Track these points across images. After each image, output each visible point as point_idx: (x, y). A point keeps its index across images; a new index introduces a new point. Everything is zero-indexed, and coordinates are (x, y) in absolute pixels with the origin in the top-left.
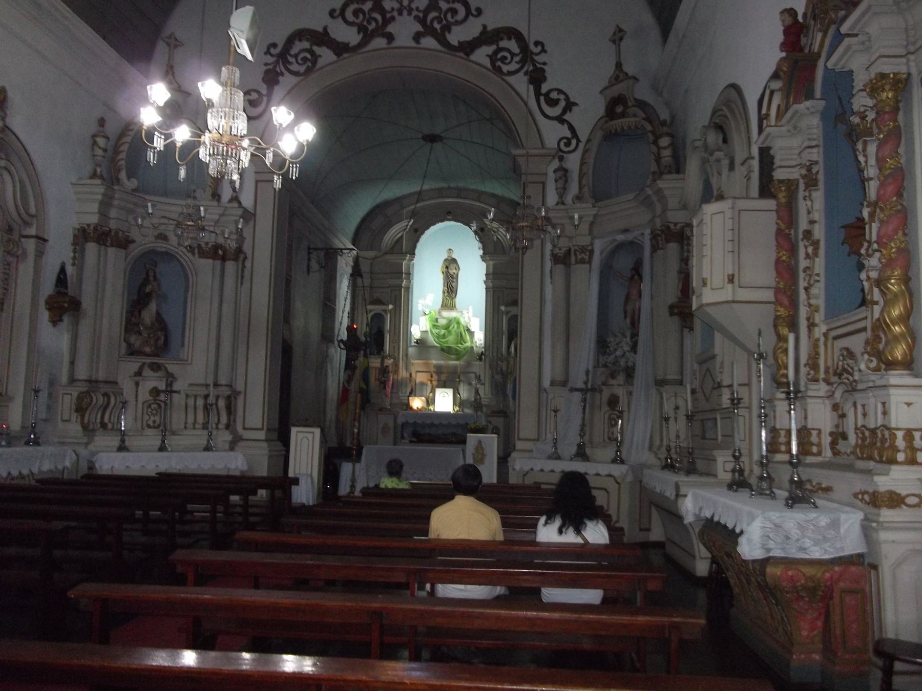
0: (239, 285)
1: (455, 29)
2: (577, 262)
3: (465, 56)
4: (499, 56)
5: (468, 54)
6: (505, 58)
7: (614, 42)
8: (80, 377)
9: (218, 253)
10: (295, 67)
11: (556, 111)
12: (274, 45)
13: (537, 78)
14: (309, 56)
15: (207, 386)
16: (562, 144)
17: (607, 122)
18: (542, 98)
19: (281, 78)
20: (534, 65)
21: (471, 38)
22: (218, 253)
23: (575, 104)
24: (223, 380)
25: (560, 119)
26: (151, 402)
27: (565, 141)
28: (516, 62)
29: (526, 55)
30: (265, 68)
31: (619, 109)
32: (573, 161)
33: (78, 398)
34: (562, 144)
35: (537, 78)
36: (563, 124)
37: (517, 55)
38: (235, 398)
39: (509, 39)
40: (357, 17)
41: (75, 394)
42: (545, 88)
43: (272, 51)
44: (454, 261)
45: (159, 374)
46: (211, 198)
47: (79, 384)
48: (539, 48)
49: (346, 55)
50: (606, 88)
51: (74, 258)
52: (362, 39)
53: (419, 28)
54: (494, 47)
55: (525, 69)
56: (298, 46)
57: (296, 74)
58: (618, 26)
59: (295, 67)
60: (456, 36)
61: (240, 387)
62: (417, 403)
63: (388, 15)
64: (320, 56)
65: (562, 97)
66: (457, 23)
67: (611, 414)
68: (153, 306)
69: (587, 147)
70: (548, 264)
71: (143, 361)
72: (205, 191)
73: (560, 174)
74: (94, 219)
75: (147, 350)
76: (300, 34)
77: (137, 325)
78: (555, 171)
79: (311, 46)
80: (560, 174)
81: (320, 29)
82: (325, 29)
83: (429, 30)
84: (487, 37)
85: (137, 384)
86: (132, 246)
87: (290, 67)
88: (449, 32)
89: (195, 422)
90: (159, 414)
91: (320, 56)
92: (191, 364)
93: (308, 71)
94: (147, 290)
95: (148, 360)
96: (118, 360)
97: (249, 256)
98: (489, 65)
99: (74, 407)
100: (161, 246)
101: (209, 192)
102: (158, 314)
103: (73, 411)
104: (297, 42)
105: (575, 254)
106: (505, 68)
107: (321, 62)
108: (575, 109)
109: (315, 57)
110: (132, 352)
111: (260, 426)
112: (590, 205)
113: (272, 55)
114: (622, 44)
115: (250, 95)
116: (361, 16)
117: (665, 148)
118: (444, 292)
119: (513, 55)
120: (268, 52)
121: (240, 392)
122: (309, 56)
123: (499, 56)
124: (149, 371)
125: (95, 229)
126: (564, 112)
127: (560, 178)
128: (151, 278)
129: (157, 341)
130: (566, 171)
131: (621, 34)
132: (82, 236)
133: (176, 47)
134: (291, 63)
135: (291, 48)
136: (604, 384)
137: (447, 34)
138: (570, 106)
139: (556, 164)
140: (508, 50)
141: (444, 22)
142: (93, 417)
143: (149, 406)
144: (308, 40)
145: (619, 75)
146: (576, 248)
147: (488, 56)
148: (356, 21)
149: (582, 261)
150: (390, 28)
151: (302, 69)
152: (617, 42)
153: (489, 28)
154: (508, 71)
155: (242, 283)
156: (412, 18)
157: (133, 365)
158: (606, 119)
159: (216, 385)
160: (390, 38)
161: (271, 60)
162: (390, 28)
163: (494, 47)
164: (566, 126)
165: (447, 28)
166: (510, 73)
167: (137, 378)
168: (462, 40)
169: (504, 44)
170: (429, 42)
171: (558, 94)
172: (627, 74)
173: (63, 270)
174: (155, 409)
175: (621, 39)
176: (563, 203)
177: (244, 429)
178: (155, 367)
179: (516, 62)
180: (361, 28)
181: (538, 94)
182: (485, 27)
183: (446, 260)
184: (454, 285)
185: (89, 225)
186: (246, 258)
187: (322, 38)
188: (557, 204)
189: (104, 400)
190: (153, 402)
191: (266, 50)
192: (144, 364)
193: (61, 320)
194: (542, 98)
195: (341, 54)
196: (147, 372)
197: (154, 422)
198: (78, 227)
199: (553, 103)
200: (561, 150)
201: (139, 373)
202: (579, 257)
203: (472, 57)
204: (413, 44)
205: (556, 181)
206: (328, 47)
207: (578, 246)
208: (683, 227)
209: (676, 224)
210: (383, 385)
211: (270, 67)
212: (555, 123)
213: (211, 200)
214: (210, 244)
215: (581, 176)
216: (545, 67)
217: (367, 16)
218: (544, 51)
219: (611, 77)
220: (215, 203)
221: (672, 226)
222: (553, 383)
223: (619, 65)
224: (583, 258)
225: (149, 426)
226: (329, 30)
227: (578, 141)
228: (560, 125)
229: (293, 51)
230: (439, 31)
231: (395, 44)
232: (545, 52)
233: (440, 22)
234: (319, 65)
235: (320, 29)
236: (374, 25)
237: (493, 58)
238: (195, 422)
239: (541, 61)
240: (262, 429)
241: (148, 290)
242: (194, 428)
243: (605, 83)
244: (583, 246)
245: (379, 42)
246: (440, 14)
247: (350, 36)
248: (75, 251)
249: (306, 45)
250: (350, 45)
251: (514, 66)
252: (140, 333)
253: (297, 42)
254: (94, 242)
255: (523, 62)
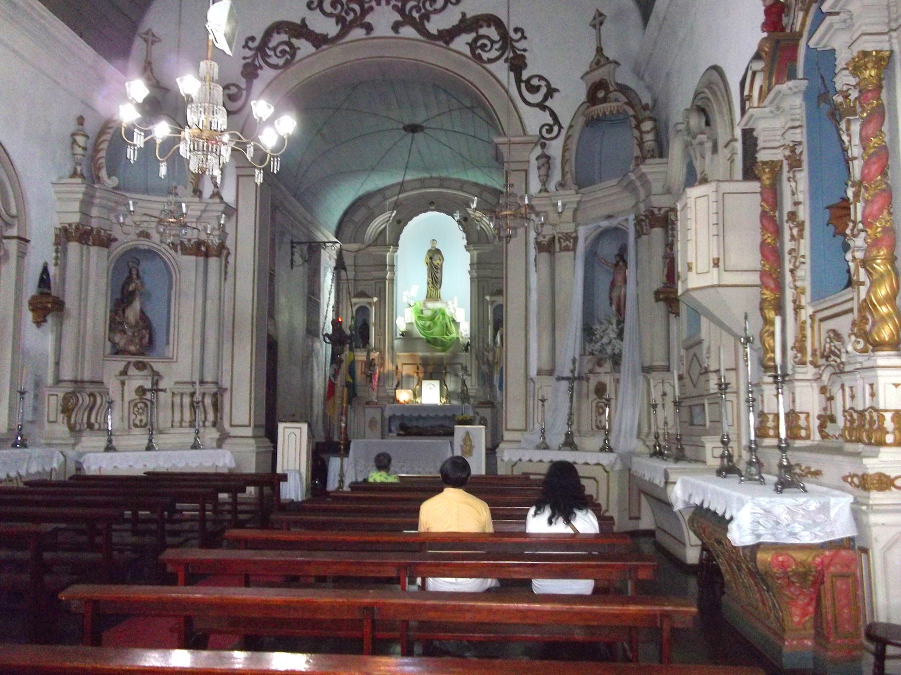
0: (223, 281)
1: (434, 17)
2: (561, 250)
3: (444, 45)
4: (479, 44)
5: (447, 43)
6: (484, 45)
7: (594, 26)
8: (66, 378)
9: (200, 249)
10: (274, 60)
11: (537, 98)
12: (252, 39)
13: (517, 65)
14: (287, 49)
15: (193, 383)
16: (544, 131)
17: (588, 107)
18: (523, 85)
19: (259, 72)
20: (514, 52)
21: (450, 27)
22: (200, 249)
23: (557, 90)
24: (209, 378)
25: (542, 106)
26: (137, 401)
27: (547, 127)
28: (496, 49)
29: (506, 42)
30: (244, 62)
31: (601, 94)
32: (555, 148)
33: (64, 398)
34: (544, 131)
35: (517, 65)
36: (544, 111)
37: (497, 42)
38: (222, 395)
39: (489, 26)
40: (335, 9)
41: (61, 395)
42: (525, 75)
43: (251, 44)
44: (438, 251)
45: (145, 372)
46: (192, 194)
47: (64, 384)
48: (519, 35)
49: (324, 47)
50: (587, 73)
51: (57, 258)
52: (341, 30)
53: (398, 17)
54: (473, 35)
55: (505, 56)
56: (278, 38)
57: (275, 67)
58: (598, 10)
59: (274, 60)
60: (435, 25)
61: (226, 384)
62: (404, 396)
63: (366, 6)
64: (299, 48)
65: (543, 83)
66: (436, 11)
67: (599, 402)
68: (137, 305)
69: (569, 134)
70: (533, 252)
71: (129, 360)
72: (186, 188)
73: (542, 161)
74: (75, 218)
75: (132, 348)
76: (278, 27)
77: (121, 323)
78: (537, 159)
79: (289, 39)
80: (542, 161)
81: (298, 21)
82: (303, 20)
83: (407, 20)
84: (467, 25)
85: (123, 383)
86: (114, 245)
87: (271, 61)
88: (428, 21)
89: (182, 420)
90: (145, 413)
91: (299, 48)
92: (176, 361)
93: (288, 64)
94: (131, 288)
95: (133, 359)
96: (103, 360)
97: (232, 251)
98: (468, 53)
99: (60, 408)
100: (144, 244)
101: (190, 188)
102: (142, 312)
103: (59, 412)
104: (275, 35)
105: (560, 242)
106: (485, 56)
107: (299, 55)
108: (556, 95)
109: (294, 50)
110: (117, 351)
111: (247, 423)
112: (573, 192)
113: (250, 49)
114: (602, 28)
115: (229, 89)
116: (339, 7)
117: (648, 132)
118: (428, 284)
119: (493, 42)
120: (246, 46)
121: (226, 389)
122: (287, 49)
123: (479, 44)
124: (135, 370)
125: (77, 228)
126: (546, 98)
127: (543, 165)
128: (135, 276)
129: (141, 339)
130: (548, 158)
131: (601, 18)
132: (64, 236)
133: (153, 43)
134: (269, 56)
135: (269, 41)
136: (591, 372)
137: (426, 23)
138: (551, 92)
139: (538, 151)
140: (488, 38)
141: (423, 11)
142: (78, 417)
143: (136, 405)
144: (286, 33)
145: (600, 59)
146: (560, 235)
147: (467, 43)
148: (334, 12)
149: (567, 249)
150: (368, 19)
151: (281, 62)
152: (598, 27)
153: (468, 16)
154: (488, 59)
155: (225, 279)
156: (390, 7)
157: (119, 364)
158: (588, 104)
159: (202, 382)
160: (369, 28)
161: (249, 53)
162: (368, 19)
163: (473, 35)
164: (547, 113)
165: (426, 17)
166: (490, 61)
167: (122, 378)
168: (441, 28)
169: (483, 31)
170: (408, 31)
171: (539, 80)
172: (608, 58)
173: (45, 270)
174: (141, 408)
175: (601, 23)
176: (546, 191)
177: (232, 426)
178: (141, 366)
179: (496, 49)
180: (340, 20)
181: (519, 81)
182: (464, 14)
183: (429, 251)
184: (438, 275)
185: (70, 225)
186: (228, 254)
187: (300, 30)
188: (540, 191)
189: (90, 400)
190: (139, 401)
191: (244, 43)
192: (129, 363)
193: (45, 321)
194: (523, 85)
195: (320, 46)
196: (133, 371)
197: (141, 421)
198: (59, 226)
199: (534, 90)
200: (543, 137)
201: (124, 372)
202: (564, 244)
203: (453, 45)
204: (392, 34)
205: (539, 168)
206: (307, 39)
207: (562, 233)
208: (667, 212)
209: (660, 209)
210: (369, 379)
211: (249, 61)
212: (537, 109)
213: (192, 197)
214: (193, 241)
215: (564, 162)
216: (526, 54)
217: (345, 7)
218: (524, 37)
219: (592, 62)
220: (197, 199)
221: (656, 211)
222: (539, 373)
223: (599, 50)
224: (567, 245)
225: (136, 426)
226: (307, 22)
227: (560, 127)
228: (541, 112)
229: (272, 44)
230: (418, 20)
231: (373, 35)
232: (525, 38)
233: (418, 11)
234: (298, 58)
235: (298, 21)
236: (352, 15)
237: (472, 46)
238: (182, 420)
239: (522, 48)
240: (249, 426)
241: (131, 288)
242: (181, 426)
243: (586, 68)
244: (567, 234)
245: (358, 33)
246: (419, 3)
247: (330, 28)
248: (57, 251)
249: (284, 37)
250: (329, 37)
251: (494, 54)
252: (124, 332)
253: (275, 35)
254: (76, 241)
255: (503, 49)
